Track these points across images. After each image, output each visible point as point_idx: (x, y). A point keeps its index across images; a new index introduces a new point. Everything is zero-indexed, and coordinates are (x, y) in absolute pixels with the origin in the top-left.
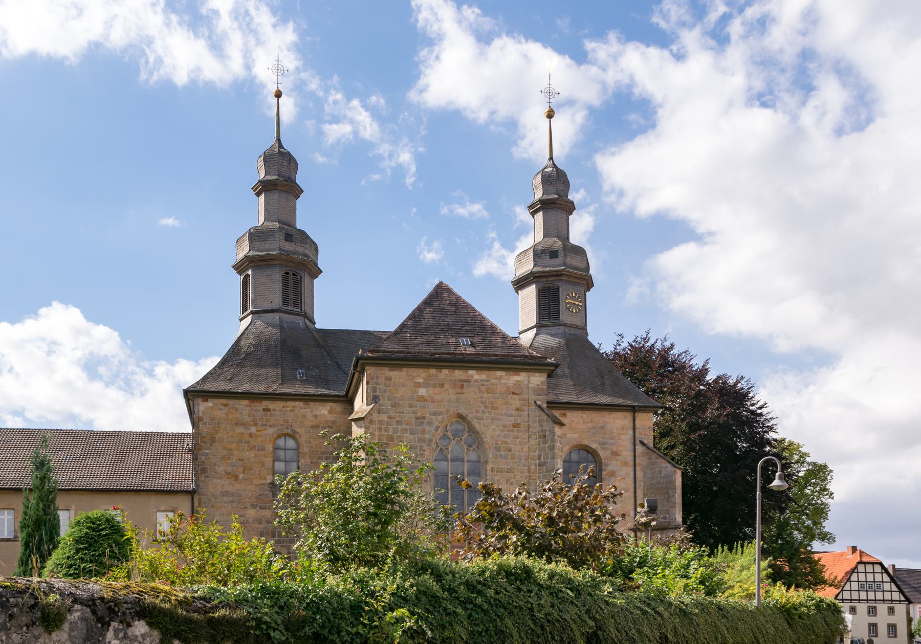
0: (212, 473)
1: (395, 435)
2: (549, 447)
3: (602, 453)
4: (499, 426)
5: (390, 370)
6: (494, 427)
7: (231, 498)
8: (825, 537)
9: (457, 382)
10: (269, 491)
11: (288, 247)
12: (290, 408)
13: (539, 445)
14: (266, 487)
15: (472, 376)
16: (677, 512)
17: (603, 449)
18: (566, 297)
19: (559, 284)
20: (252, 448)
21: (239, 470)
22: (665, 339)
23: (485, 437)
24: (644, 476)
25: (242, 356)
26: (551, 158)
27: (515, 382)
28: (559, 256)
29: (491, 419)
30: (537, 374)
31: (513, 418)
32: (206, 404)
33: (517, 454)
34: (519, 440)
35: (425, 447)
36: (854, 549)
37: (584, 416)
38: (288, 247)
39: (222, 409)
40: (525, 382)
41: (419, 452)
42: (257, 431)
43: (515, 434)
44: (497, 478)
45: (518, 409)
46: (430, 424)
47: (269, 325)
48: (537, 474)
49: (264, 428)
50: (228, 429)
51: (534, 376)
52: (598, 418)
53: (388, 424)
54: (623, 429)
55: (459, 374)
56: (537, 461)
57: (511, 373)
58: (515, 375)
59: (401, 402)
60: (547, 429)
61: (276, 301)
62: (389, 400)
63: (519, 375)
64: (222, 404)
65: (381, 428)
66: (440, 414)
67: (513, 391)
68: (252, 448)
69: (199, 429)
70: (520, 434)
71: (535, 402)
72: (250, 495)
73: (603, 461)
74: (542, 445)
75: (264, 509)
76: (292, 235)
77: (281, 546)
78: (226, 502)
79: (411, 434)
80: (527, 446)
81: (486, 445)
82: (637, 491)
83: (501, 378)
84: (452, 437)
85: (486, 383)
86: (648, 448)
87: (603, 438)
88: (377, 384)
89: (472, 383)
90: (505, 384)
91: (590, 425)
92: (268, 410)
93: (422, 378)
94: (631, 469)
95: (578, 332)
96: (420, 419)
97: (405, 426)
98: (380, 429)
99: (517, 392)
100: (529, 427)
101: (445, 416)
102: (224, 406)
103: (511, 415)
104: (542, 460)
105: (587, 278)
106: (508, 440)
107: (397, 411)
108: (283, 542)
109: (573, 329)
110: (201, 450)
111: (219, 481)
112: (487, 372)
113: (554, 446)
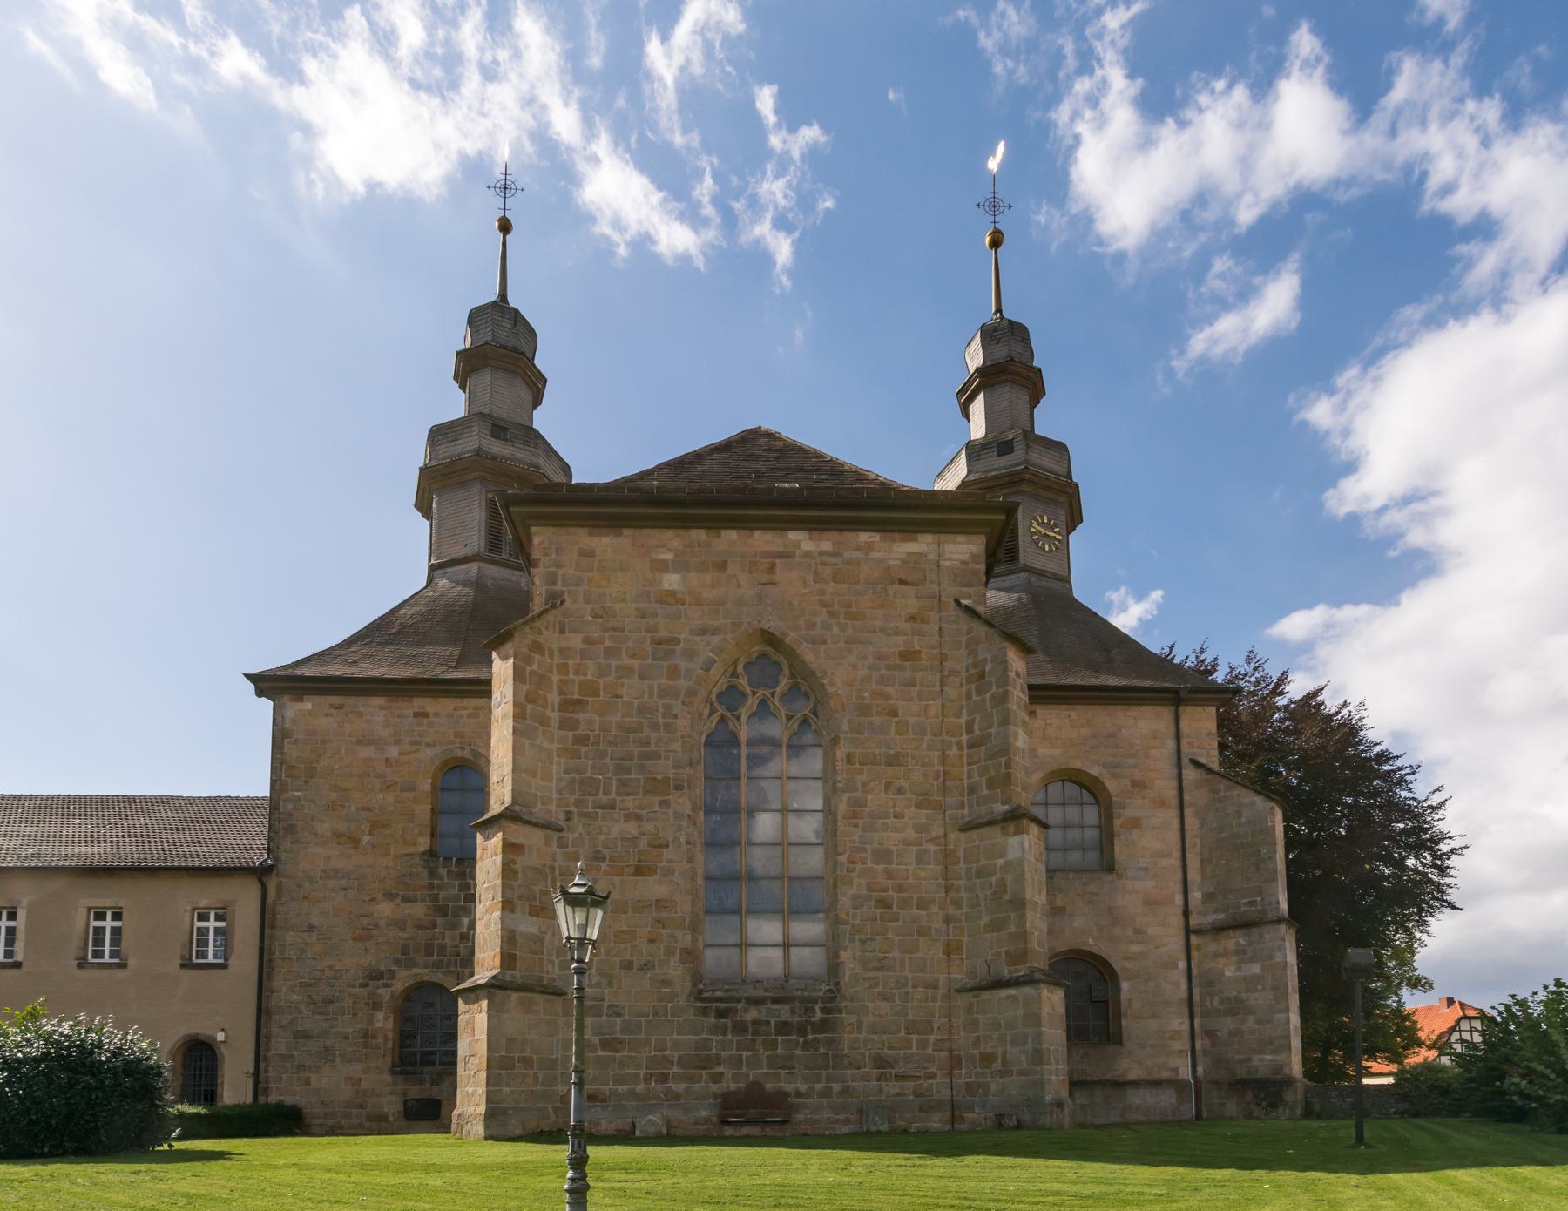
0: (307, 834)
1: (601, 681)
2: (993, 698)
3: (1111, 785)
4: (865, 658)
5: (591, 534)
6: (852, 658)
7: (343, 882)
8: (1416, 983)
9: (758, 559)
10: (422, 867)
11: (498, 448)
12: (470, 711)
13: (969, 697)
14: (417, 860)
15: (797, 545)
16: (1280, 890)
17: (1115, 776)
18: (1033, 525)
19: (1018, 499)
20: (388, 787)
21: (363, 827)
22: (1202, 651)
23: (832, 684)
24: (1202, 826)
25: (394, 630)
26: (999, 310)
27: (904, 557)
28: (1016, 449)
29: (846, 642)
30: (960, 538)
31: (900, 639)
32: (299, 706)
33: (912, 720)
34: (916, 689)
35: (678, 708)
36: (1450, 1001)
37: (1073, 714)
38: (498, 448)
39: (331, 715)
40: (931, 557)
41: (661, 720)
42: (400, 754)
43: (908, 674)
44: (860, 778)
45: (912, 618)
46: (690, 654)
47: (458, 583)
48: (965, 769)
49: (415, 748)
50: (343, 751)
51: (954, 543)
52: (1103, 718)
53: (584, 655)
54: (1154, 737)
55: (763, 540)
56: (965, 737)
57: (896, 535)
58: (905, 540)
59: (617, 606)
60: (989, 657)
61: (475, 540)
62: (587, 601)
63: (915, 540)
64: (331, 705)
65: (566, 665)
66: (715, 631)
67: (901, 576)
68: (388, 787)
69: (282, 753)
70: (919, 675)
71: (957, 602)
72: (383, 874)
73: (1114, 799)
74: (975, 698)
75: (411, 901)
76: (507, 429)
77: (443, 973)
78: (333, 890)
79: (642, 678)
80: (939, 702)
81: (832, 703)
82: (1189, 855)
83: (869, 547)
84: (748, 689)
85: (833, 560)
86: (1209, 771)
87: (1114, 756)
88: (559, 565)
89: (798, 559)
90: (880, 561)
91: (1085, 731)
92: (426, 715)
93: (670, 550)
94: (1173, 814)
95: (1055, 585)
96: (664, 646)
97: (627, 661)
98: (563, 669)
99: (910, 579)
100: (943, 658)
101: (729, 636)
102: (336, 708)
103: (897, 633)
104: (977, 732)
105: (1071, 491)
106: (889, 690)
107: (609, 625)
108: (448, 965)
109: (1044, 579)
110: (286, 791)
111: (320, 850)
112: (835, 535)
113: (1006, 693)
